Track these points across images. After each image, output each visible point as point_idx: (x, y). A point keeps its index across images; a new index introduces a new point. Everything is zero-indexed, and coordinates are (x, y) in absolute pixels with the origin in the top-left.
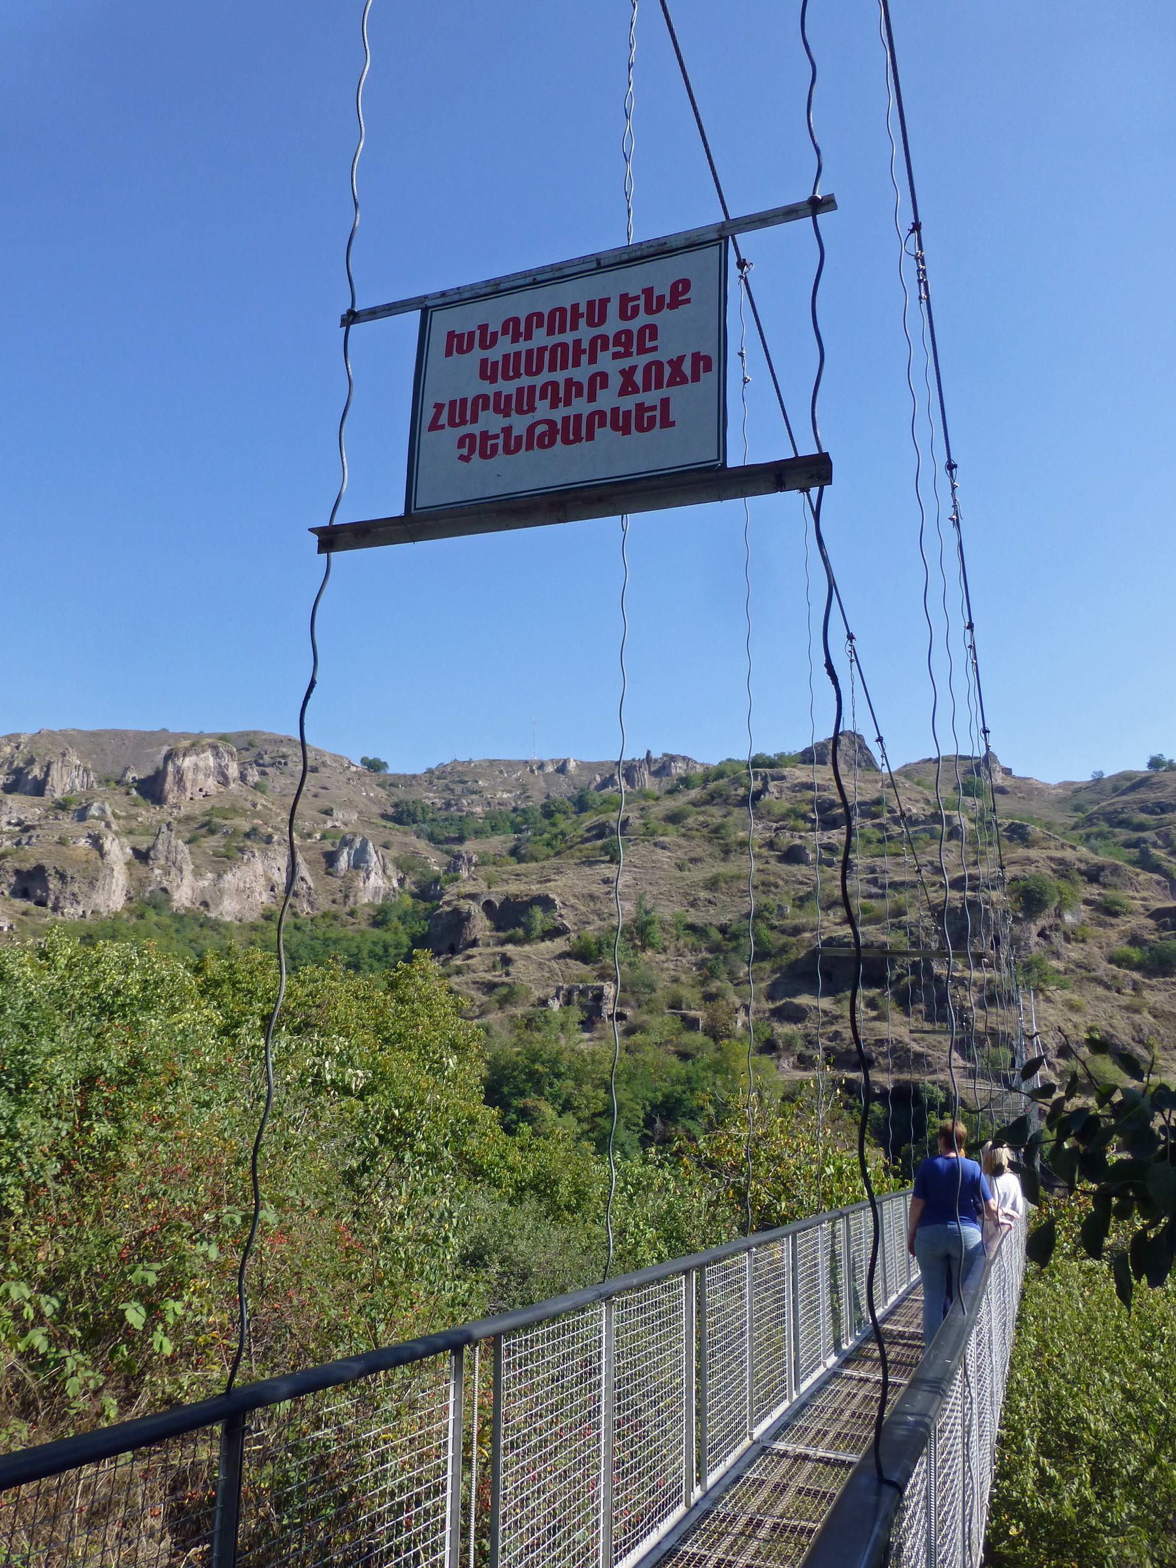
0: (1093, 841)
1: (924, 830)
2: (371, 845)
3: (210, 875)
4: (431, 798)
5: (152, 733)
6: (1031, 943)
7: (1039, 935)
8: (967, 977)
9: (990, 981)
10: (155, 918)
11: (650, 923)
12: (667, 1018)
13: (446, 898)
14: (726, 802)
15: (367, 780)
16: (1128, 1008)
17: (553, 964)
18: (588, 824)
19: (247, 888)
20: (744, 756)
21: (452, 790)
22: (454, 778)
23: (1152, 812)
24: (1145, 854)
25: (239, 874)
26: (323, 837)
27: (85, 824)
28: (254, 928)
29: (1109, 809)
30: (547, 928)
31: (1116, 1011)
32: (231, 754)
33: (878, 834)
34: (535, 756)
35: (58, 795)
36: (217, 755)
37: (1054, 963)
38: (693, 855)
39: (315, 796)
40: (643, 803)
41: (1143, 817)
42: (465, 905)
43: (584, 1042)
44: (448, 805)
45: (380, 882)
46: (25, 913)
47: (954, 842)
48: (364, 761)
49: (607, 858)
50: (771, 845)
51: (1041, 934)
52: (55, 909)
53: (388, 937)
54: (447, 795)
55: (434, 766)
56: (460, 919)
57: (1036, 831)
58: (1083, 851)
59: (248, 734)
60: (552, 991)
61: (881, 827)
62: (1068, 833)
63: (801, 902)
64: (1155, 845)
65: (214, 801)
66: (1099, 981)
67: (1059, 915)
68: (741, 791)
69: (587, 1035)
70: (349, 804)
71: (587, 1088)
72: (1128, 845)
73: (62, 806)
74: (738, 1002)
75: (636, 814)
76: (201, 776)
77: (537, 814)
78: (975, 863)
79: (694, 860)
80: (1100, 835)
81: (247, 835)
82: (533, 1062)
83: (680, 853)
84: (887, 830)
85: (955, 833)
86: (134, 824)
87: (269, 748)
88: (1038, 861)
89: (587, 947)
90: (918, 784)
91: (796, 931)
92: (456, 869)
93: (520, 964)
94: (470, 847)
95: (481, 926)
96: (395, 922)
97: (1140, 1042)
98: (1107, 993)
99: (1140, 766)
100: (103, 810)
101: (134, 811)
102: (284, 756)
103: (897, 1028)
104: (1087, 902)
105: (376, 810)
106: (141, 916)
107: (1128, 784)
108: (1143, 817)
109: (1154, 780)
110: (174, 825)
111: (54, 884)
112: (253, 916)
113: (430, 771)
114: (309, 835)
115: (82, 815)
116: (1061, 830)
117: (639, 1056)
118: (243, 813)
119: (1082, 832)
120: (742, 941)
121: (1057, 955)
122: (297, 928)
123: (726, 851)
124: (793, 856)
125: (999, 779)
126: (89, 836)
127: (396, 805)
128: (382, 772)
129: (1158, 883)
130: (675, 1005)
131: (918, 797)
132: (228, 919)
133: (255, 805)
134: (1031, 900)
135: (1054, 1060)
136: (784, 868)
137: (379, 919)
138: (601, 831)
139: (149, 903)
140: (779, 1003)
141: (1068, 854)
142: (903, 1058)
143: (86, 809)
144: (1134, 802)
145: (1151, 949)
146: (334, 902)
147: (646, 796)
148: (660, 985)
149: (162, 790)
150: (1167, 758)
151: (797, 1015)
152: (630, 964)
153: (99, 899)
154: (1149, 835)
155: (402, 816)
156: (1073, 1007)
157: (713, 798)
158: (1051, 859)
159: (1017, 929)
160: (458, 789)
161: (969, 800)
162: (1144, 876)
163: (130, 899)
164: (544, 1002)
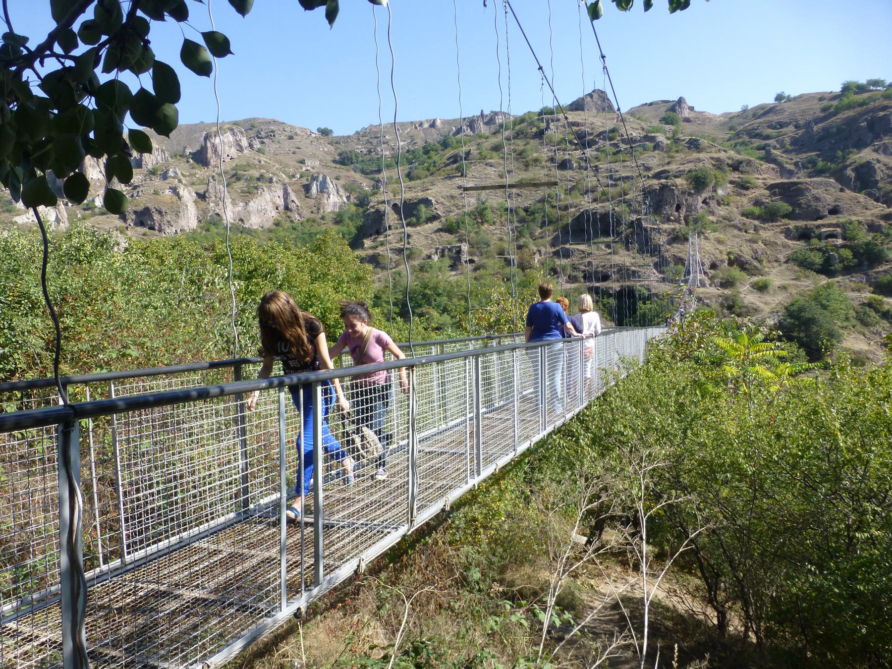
0: (738, 147)
1: (640, 146)
2: (328, 178)
3: (241, 204)
4: (360, 149)
5: (195, 125)
6: (698, 207)
7: (703, 202)
8: (660, 230)
9: (674, 230)
10: (216, 230)
11: (485, 209)
12: (496, 260)
13: (372, 204)
14: (526, 137)
15: (322, 141)
16: (750, 241)
17: (433, 236)
18: (448, 155)
19: (263, 209)
20: (537, 109)
21: (371, 143)
22: (371, 136)
23: (775, 128)
24: (768, 153)
25: (257, 202)
26: (301, 177)
27: (167, 181)
28: (270, 231)
29: (750, 128)
30: (428, 216)
31: (743, 242)
32: (242, 133)
33: (614, 150)
34: (417, 118)
35: (150, 167)
36: (234, 134)
37: (711, 218)
38: (509, 169)
39: (294, 153)
40: (479, 141)
41: (769, 131)
42: (381, 207)
43: (452, 276)
44: (370, 152)
45: (336, 199)
46: (144, 235)
47: (657, 152)
48: (319, 130)
49: (459, 174)
50: (552, 160)
51: (704, 202)
52: (160, 231)
53: (344, 229)
54: (369, 146)
55: (359, 130)
56: (379, 216)
57: (704, 142)
58: (732, 153)
59: (250, 120)
60: (433, 251)
61: (616, 145)
62: (725, 143)
63: (569, 191)
64: (775, 148)
65: (236, 162)
66: (735, 227)
67: (715, 191)
68: (534, 130)
69: (453, 273)
70: (313, 156)
71: (455, 300)
72: (759, 148)
73: (153, 173)
74: (535, 249)
75: (475, 148)
76: (227, 148)
77: (421, 153)
78: (669, 163)
79: (509, 172)
80: (743, 144)
81: (258, 179)
82: (425, 288)
83: (501, 168)
84: (618, 147)
85: (657, 146)
86: (194, 179)
87: (264, 128)
88: (704, 160)
89: (451, 225)
90: (639, 119)
91: (566, 208)
92: (378, 188)
93: (415, 237)
94: (385, 175)
95: (391, 218)
96: (347, 221)
97: (756, 259)
98: (739, 233)
99: (770, 100)
100: (176, 173)
101: (193, 171)
102: (272, 132)
103: (624, 258)
104: (731, 182)
105: (330, 158)
106: (208, 230)
107: (762, 112)
108: (769, 131)
109: (778, 108)
110: (216, 177)
111: (156, 217)
112: (269, 224)
113: (357, 133)
114: (293, 176)
115: (165, 176)
116: (721, 142)
117: (482, 281)
118: (254, 167)
119: (733, 142)
120: (537, 215)
121: (712, 213)
122: (294, 229)
123: (527, 165)
124: (564, 165)
125: (686, 113)
126: (170, 188)
127: (340, 155)
128: (330, 136)
129: (773, 169)
130: (501, 253)
131: (638, 126)
132: (255, 227)
133: (260, 162)
134: (699, 182)
135: (708, 271)
136: (559, 173)
137: (338, 220)
138: (455, 159)
139: (211, 222)
140: (557, 248)
141: (722, 155)
142: (625, 272)
143: (166, 172)
144: (765, 123)
145: (766, 207)
146: (312, 212)
147: (480, 137)
148: (493, 242)
149: (206, 158)
150: (786, 94)
151: (567, 254)
152: (476, 233)
153: (183, 223)
154: (772, 142)
155: (344, 160)
156: (720, 242)
157: (518, 135)
158: (712, 158)
159: (690, 199)
160: (375, 141)
161: (667, 127)
162: (765, 166)
163: (200, 221)
164: (429, 257)
